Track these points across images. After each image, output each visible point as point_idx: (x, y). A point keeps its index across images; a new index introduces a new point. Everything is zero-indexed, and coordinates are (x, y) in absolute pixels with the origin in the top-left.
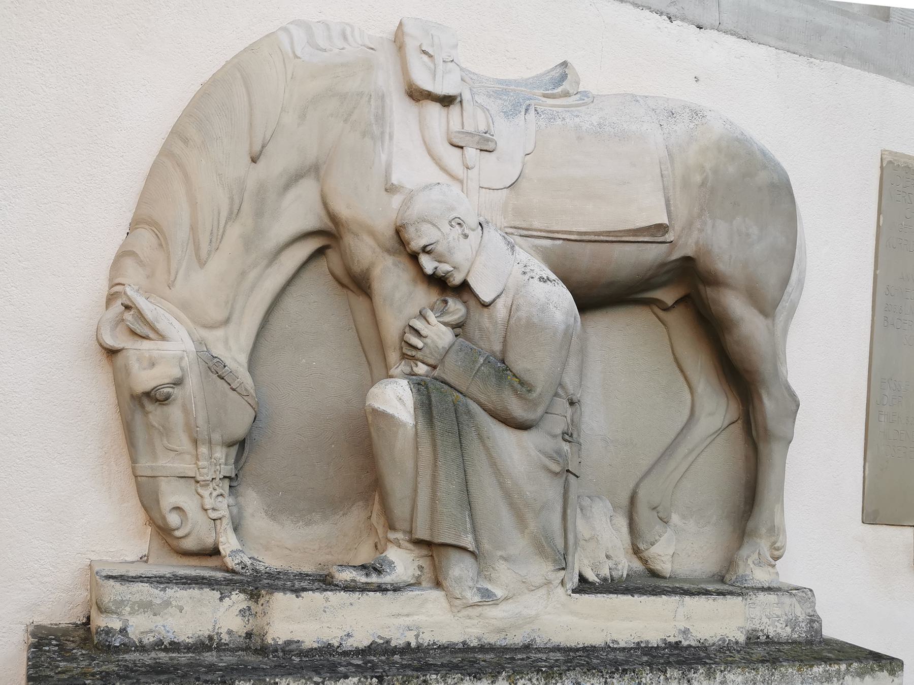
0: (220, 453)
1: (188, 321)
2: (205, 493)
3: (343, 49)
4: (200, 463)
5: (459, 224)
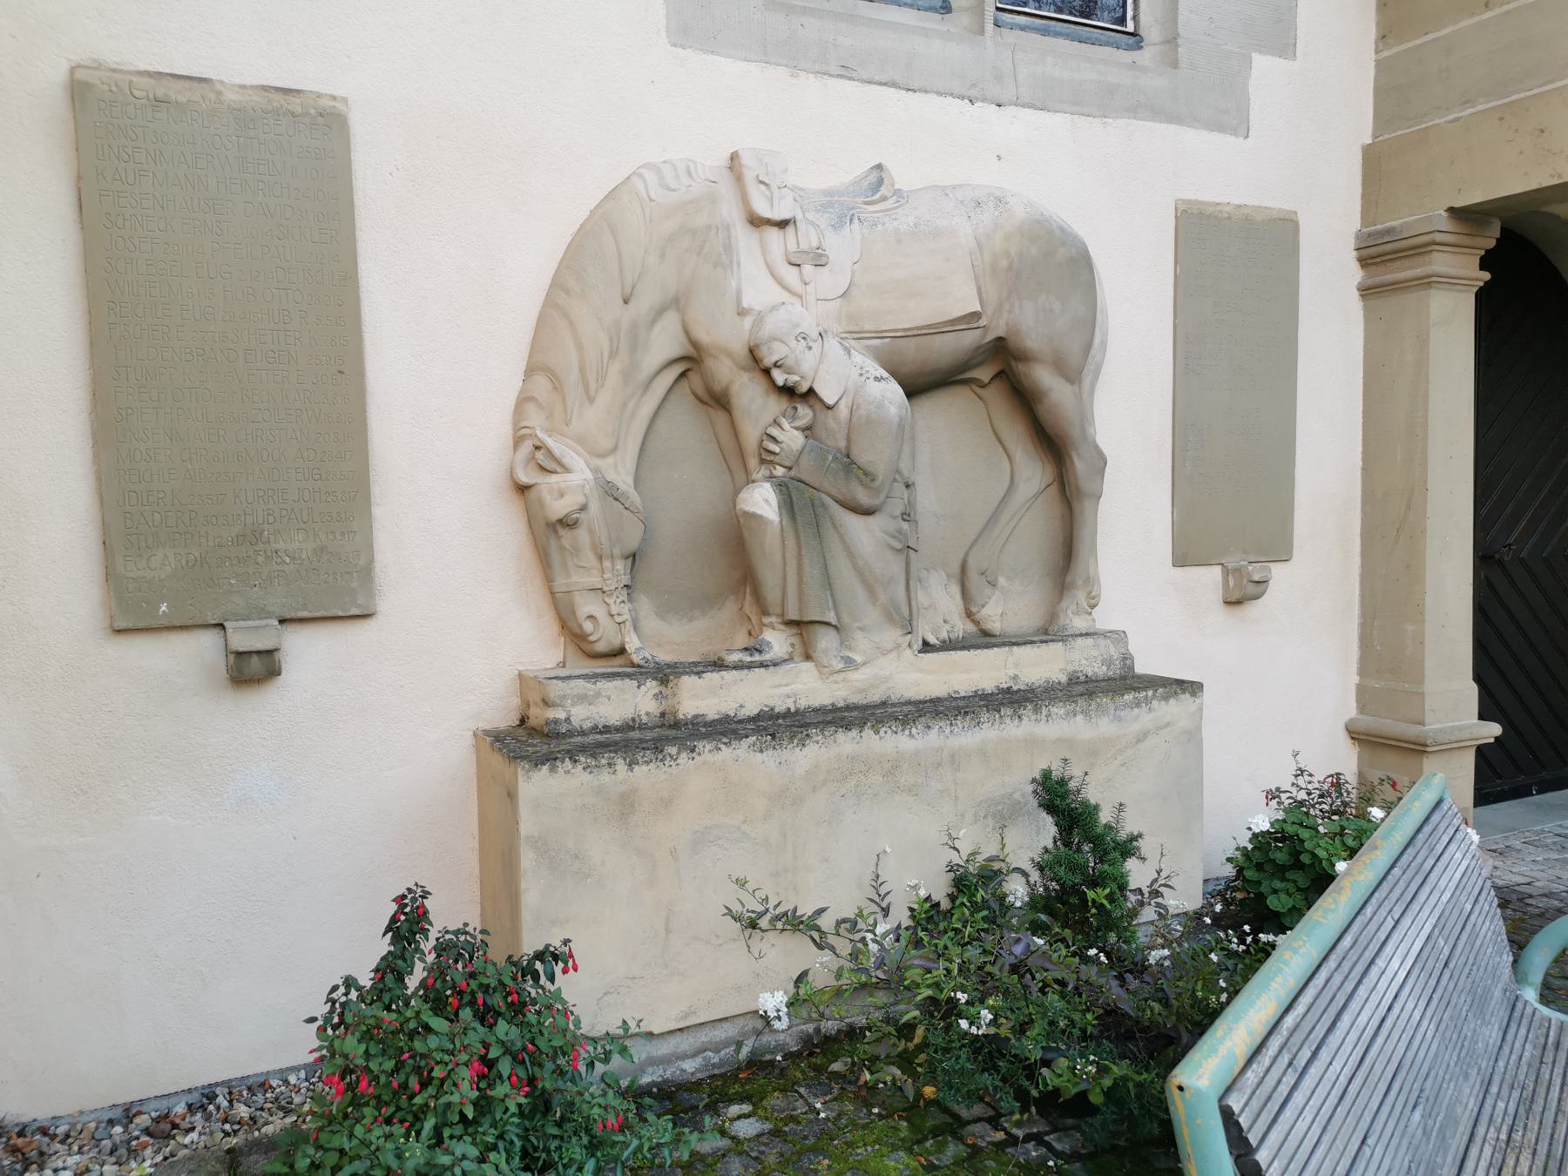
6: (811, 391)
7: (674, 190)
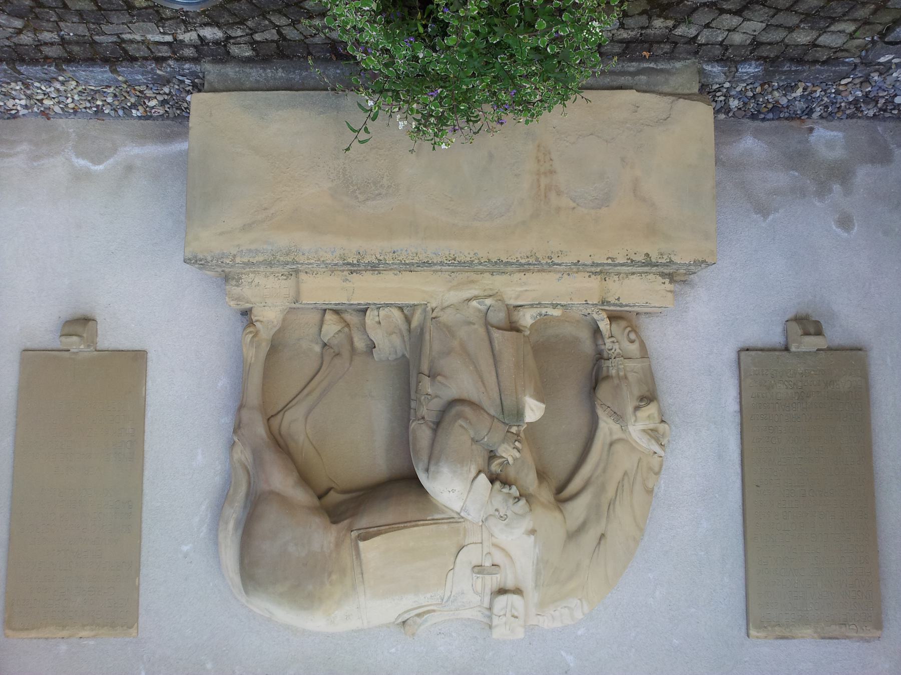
0: (613, 372)
1: (632, 442)
2: (618, 351)
3: (555, 611)
4: (623, 366)
5: (502, 517)
6: (492, 481)
7: (565, 607)
